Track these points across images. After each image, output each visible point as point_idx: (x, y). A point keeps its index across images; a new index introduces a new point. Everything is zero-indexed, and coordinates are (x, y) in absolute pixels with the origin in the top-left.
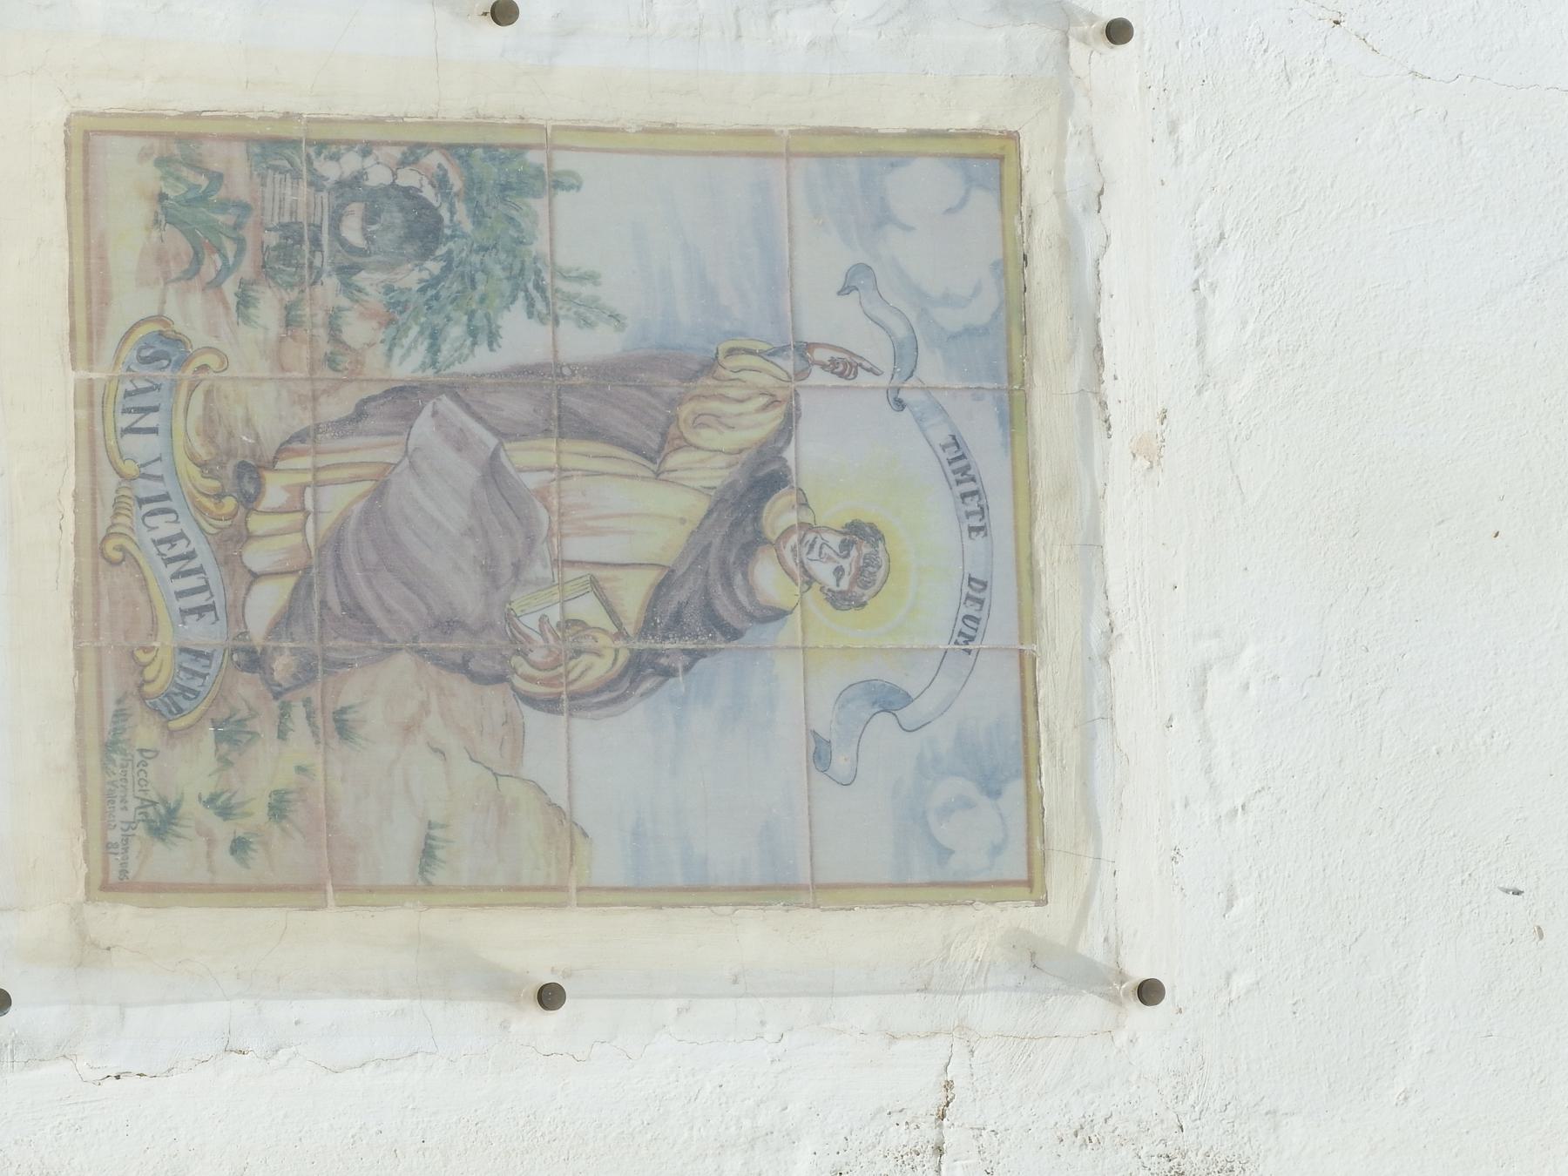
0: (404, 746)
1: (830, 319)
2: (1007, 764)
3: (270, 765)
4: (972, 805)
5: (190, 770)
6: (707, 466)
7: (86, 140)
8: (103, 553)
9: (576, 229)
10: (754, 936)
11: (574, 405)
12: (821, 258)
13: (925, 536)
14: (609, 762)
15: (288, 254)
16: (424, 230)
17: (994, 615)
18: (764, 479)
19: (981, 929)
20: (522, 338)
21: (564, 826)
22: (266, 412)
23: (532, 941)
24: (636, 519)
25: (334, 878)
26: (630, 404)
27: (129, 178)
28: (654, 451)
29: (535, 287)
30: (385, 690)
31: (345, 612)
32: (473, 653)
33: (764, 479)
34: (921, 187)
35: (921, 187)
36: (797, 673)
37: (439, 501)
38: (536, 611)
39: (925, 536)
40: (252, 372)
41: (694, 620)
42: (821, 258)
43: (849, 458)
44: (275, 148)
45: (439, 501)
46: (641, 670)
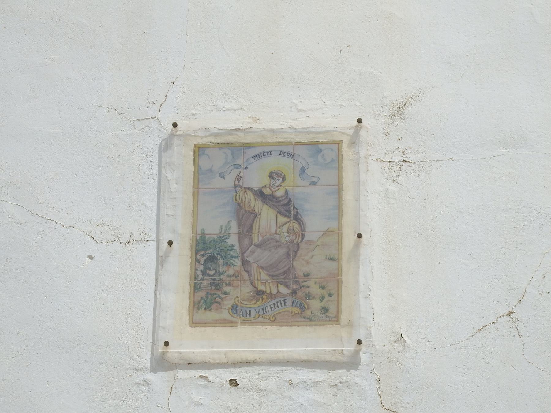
0: (310, 263)
2: (315, 148)
3: (314, 289)
4: (323, 154)
5: (315, 305)
6: (258, 205)
7: (194, 323)
8: (274, 321)
9: (213, 230)
10: (348, 197)
13: (273, 163)
14: (314, 224)
15: (216, 285)
17: (287, 150)
18: (260, 194)
19: (347, 153)
20: (233, 240)
24: (268, 219)
26: (246, 219)
27: (202, 315)
28: (255, 215)
29: (223, 238)
31: (285, 274)
32: (293, 250)
34: (205, 163)
35: (205, 163)
36: (298, 188)
37: (264, 257)
39: (273, 163)
40: (239, 292)
41: (287, 208)
43: (256, 178)
44: (196, 287)
45: (264, 257)
46: (297, 218)
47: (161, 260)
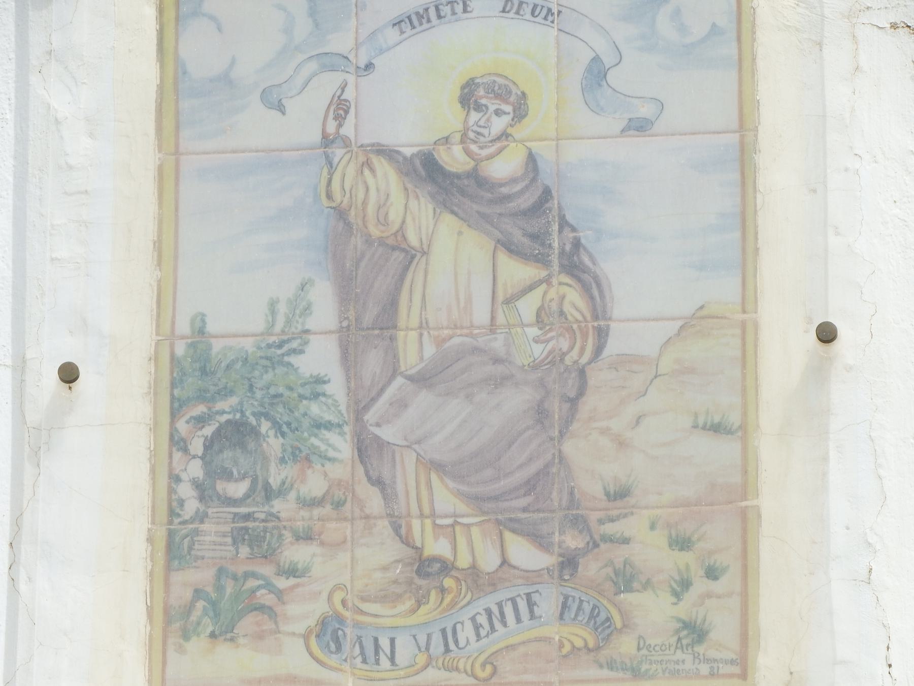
0: (633, 447)
1: (304, 120)
3: (650, 550)
5: (654, 611)
9: (237, 315)
10: (779, 175)
11: (370, 322)
12: (257, 128)
14: (646, 289)
16: (238, 433)
18: (427, 171)
20: (320, 358)
21: (696, 323)
22: (378, 554)
23: (784, 346)
25: (736, 501)
26: (370, 275)
28: (406, 255)
29: (280, 349)
30: (591, 462)
31: (529, 491)
32: (562, 394)
33: (427, 171)
36: (576, 144)
37: (445, 422)
38: (530, 346)
40: (349, 565)
41: (535, 224)
42: (257, 128)
44: (175, 548)
45: (445, 422)
46: (575, 264)
47: (34, 443)
